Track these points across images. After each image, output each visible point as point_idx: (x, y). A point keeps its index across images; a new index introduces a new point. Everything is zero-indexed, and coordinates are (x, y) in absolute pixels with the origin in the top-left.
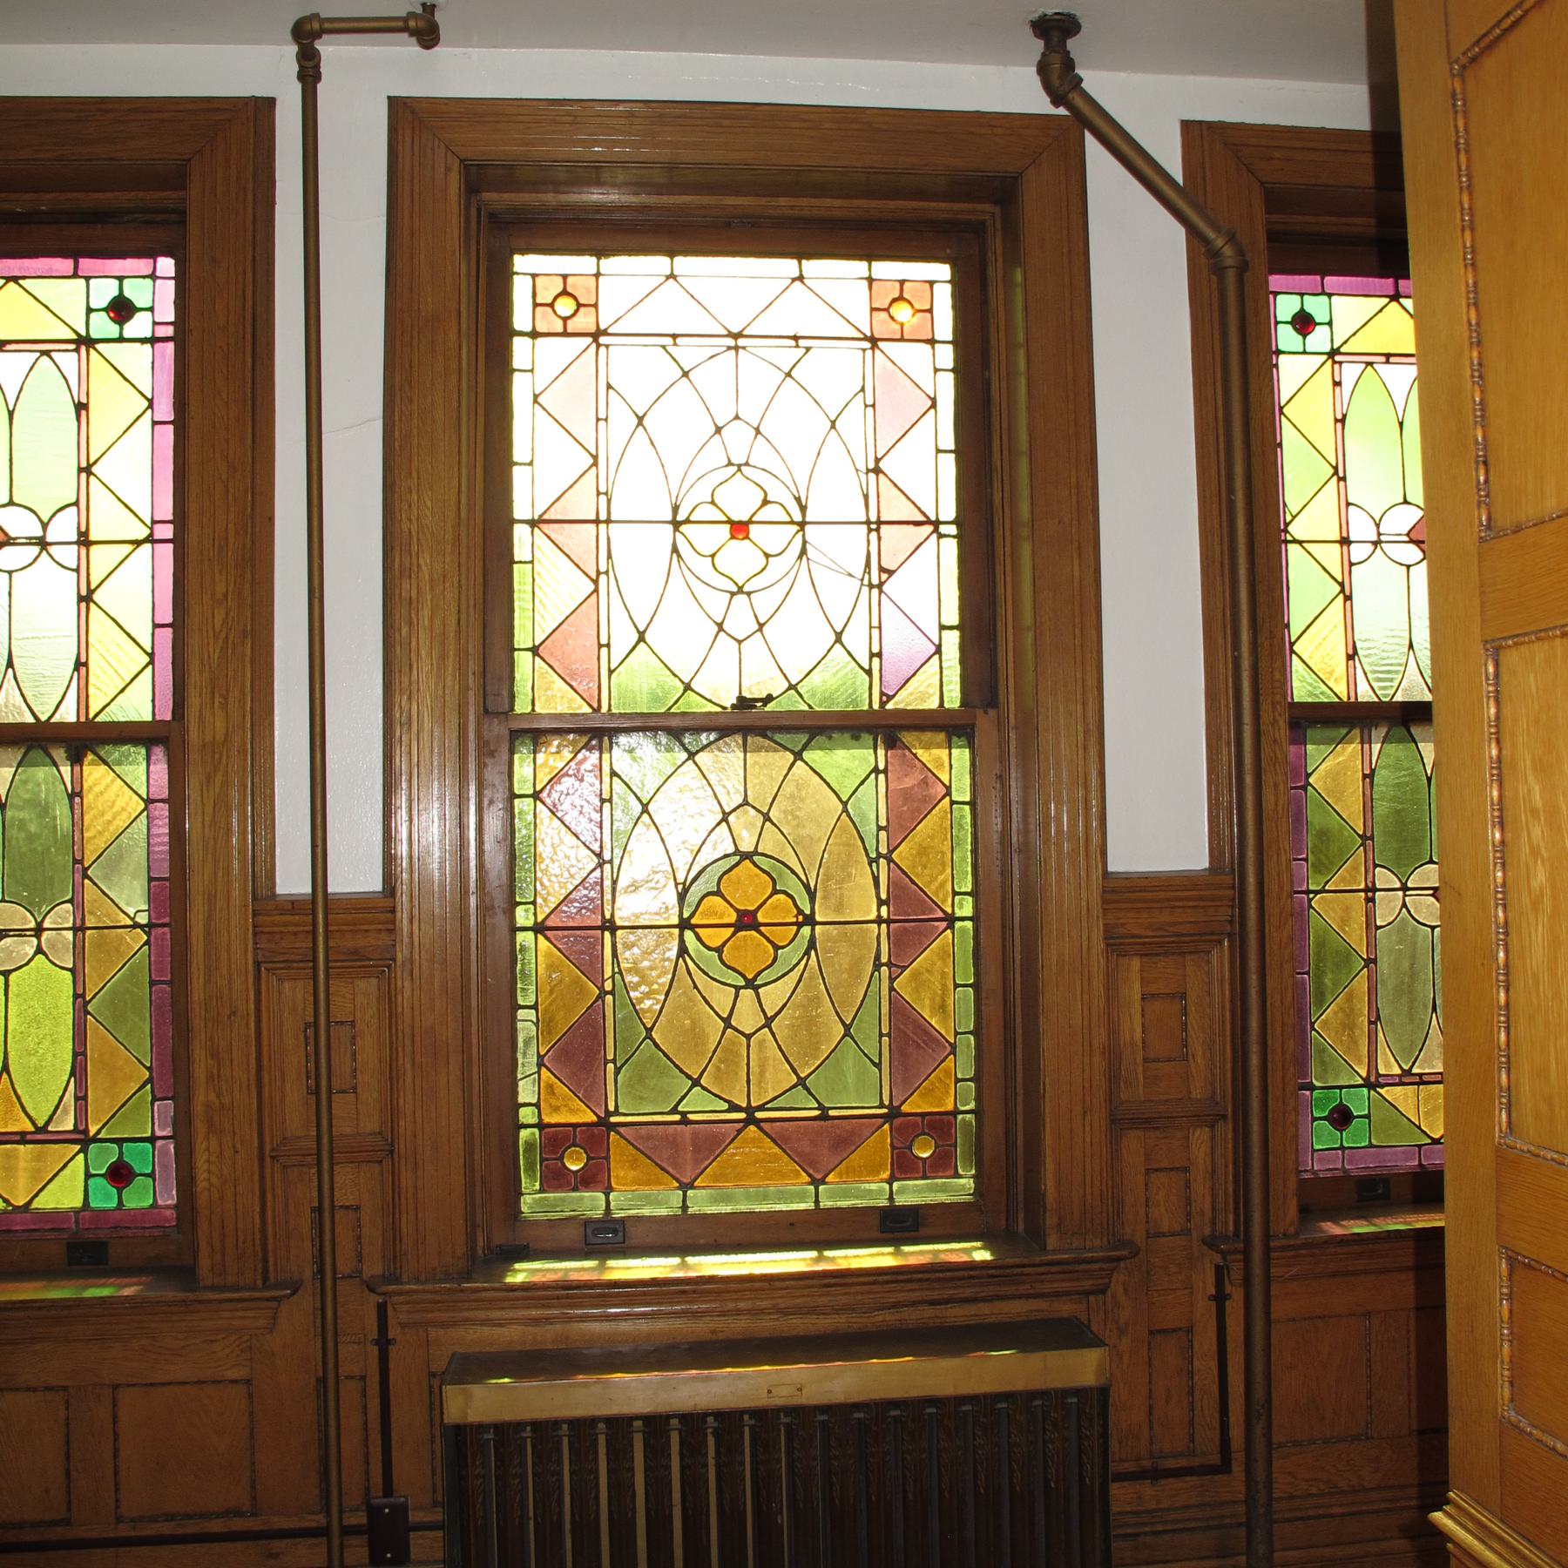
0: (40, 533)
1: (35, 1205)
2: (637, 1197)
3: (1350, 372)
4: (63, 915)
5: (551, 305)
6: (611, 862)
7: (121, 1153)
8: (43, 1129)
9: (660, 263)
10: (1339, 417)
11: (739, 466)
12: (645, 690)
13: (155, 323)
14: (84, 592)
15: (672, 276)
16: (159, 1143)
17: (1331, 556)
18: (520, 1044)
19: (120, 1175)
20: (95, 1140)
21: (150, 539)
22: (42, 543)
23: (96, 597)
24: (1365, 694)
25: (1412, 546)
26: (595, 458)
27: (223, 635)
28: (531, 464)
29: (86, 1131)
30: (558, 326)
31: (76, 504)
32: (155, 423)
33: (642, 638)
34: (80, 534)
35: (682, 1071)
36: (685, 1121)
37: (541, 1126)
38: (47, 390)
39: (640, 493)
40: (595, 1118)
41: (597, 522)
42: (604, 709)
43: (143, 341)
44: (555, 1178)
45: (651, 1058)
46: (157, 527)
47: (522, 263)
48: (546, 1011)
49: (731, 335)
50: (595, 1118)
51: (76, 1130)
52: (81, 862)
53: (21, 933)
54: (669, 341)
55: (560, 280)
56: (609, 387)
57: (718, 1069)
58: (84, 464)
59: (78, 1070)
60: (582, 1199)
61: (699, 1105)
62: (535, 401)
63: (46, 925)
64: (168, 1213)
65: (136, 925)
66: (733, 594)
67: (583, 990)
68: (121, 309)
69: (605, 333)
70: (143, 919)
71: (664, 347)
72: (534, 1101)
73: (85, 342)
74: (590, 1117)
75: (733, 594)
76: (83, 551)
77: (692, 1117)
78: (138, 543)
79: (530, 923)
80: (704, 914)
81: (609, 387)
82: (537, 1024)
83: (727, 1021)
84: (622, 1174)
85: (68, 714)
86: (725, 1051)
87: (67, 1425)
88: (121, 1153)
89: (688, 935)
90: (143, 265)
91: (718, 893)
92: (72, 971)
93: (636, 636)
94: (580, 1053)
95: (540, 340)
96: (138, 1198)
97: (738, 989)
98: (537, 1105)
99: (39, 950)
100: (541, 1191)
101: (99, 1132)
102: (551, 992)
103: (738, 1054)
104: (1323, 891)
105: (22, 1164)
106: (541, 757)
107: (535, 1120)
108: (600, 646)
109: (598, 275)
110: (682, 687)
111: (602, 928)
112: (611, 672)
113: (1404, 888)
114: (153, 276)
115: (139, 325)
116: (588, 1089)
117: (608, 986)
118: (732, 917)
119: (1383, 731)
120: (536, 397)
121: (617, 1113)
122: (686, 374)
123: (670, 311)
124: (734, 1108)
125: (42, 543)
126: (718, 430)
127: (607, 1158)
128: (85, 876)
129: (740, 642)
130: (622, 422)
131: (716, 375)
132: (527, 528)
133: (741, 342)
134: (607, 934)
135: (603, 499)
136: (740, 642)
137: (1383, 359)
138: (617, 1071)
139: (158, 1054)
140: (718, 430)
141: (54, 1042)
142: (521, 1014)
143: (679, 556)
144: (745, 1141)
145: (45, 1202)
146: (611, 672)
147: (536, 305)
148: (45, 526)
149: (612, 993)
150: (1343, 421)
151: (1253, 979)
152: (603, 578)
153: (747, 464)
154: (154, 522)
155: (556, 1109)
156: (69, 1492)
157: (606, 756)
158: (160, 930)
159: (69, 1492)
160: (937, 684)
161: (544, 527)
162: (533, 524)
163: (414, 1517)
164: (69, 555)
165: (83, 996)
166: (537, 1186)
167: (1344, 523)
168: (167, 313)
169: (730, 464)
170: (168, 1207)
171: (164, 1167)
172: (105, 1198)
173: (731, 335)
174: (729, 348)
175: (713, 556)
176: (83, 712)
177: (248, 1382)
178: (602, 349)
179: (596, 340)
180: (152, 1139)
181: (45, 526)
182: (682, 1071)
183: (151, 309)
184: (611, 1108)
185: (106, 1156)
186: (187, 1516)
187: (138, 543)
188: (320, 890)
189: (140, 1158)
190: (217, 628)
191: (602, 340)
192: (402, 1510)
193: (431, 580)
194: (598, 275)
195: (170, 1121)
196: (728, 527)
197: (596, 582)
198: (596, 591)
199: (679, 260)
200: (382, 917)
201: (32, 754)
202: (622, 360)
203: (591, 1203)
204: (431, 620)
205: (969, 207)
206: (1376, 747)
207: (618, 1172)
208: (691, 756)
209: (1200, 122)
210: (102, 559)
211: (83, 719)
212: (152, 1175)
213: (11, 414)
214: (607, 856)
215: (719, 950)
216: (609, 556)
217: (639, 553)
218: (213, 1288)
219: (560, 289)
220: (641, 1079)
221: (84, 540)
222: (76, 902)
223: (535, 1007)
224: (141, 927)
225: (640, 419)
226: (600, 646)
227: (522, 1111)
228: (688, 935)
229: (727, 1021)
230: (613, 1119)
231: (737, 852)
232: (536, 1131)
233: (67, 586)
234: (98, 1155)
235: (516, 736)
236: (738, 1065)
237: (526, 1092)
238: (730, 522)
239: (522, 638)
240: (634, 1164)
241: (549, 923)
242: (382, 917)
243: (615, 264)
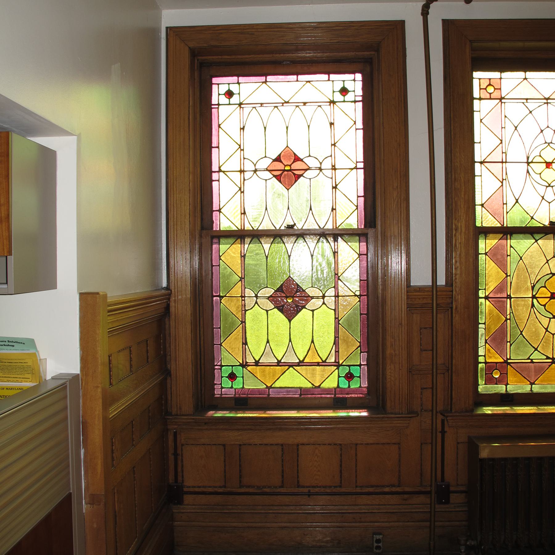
0: (319, 166)
1: (321, 386)
2: (516, 386)
3: (247, 109)
4: (331, 292)
5: (485, 89)
6: (510, 276)
7: (350, 370)
8: (325, 362)
9: (521, 74)
10: (242, 127)
11: (549, 143)
12: (518, 219)
13: (355, 96)
14: (334, 186)
15: (525, 79)
16: (362, 367)
17: (236, 177)
18: (480, 336)
19: (349, 377)
20: (341, 365)
21: (356, 168)
22: (320, 169)
23: (338, 187)
24: (248, 227)
25: (268, 172)
26: (501, 141)
27: (396, 200)
28: (480, 143)
29: (338, 362)
30: (488, 96)
31: (331, 156)
32: (356, 129)
33: (517, 202)
34: (333, 166)
35: (531, 345)
36: (532, 362)
37: (486, 363)
38: (320, 118)
39: (516, 153)
40: (503, 361)
41: (502, 162)
42: (505, 225)
43: (352, 102)
44: (490, 380)
45: (522, 341)
46: (358, 164)
47: (476, 74)
48: (488, 325)
49: (545, 99)
50: (503, 361)
51: (335, 362)
52: (337, 274)
53: (318, 298)
54: (525, 101)
55: (488, 80)
56: (505, 117)
57: (543, 345)
58: (333, 143)
59: (336, 343)
60: (498, 387)
61: (537, 356)
62: (481, 122)
63: (326, 295)
64: (365, 389)
65: (356, 295)
66: (547, 187)
67: (499, 318)
68: (344, 91)
69: (504, 98)
70: (358, 293)
71: (523, 103)
72: (484, 354)
73: (333, 102)
74: (502, 360)
75: (547, 187)
76: (334, 171)
77: (534, 361)
78: (352, 169)
79: (484, 296)
80: (540, 294)
81: (505, 117)
82: (485, 329)
83: (546, 329)
84: (511, 379)
85: (330, 226)
86: (546, 339)
87: (341, 456)
88: (350, 370)
89: (535, 300)
90: (351, 76)
91: (545, 287)
92: (335, 310)
93: (515, 201)
94: (499, 339)
95: (482, 101)
96: (355, 384)
97: (550, 318)
98: (485, 356)
99: (324, 303)
100: (485, 384)
101: (343, 362)
102: (490, 319)
103: (549, 340)
104: (225, 296)
105: (318, 373)
106: (487, 241)
107: (484, 361)
108: (504, 204)
109: (501, 78)
110: (530, 218)
111: (507, 298)
112: (507, 213)
113: (256, 296)
114: (354, 80)
115: (350, 97)
116: (501, 351)
117: (508, 317)
118: (549, 295)
119: (249, 240)
120: (481, 120)
121: (510, 359)
122: (531, 112)
123: (524, 91)
124: (548, 358)
125: (320, 169)
126: (542, 131)
127: (507, 374)
128: (339, 279)
129: (550, 203)
130: (510, 128)
131: (541, 112)
132: (479, 164)
133: (549, 101)
134: (508, 300)
135: (504, 154)
136: (550, 203)
137: (260, 105)
138: (511, 345)
139: (363, 338)
140: (542, 131)
141: (328, 333)
142: (480, 326)
143: (529, 174)
144: (551, 369)
145: (325, 385)
146: (507, 213)
147: (480, 89)
148: (321, 163)
149: (510, 319)
150: (243, 129)
151: (435, 323)
152: (504, 181)
153: (551, 143)
154: (357, 162)
155: (490, 357)
156: (341, 477)
157: (509, 241)
158: (363, 297)
159: (341, 477)
160: (352, 219)
161: (486, 164)
162: (481, 163)
163: (452, 489)
164: (329, 173)
165: (338, 318)
166: (484, 383)
167: (242, 163)
168: (359, 92)
169: (546, 143)
170: (365, 387)
171: (364, 374)
172: (344, 384)
173: (545, 99)
174: (545, 103)
175: (540, 174)
176: (335, 225)
177: (399, 444)
178: (503, 104)
179: (501, 101)
180: (360, 365)
181: (321, 163)
182: (531, 345)
183: (354, 91)
184: (508, 357)
185: (344, 371)
186: (377, 486)
187: (352, 169)
188: (435, 284)
189: (356, 371)
190: (395, 198)
191: (503, 101)
192: (448, 486)
193: (464, 182)
194: (501, 78)
195: (366, 359)
196: (545, 164)
197: (502, 182)
198: (502, 185)
199: (528, 73)
200: (448, 293)
201: (254, 240)
202: (510, 108)
203: (501, 389)
204: (464, 195)
205: (366, 52)
206: (246, 246)
207: (510, 378)
208: (536, 241)
209: (448, 20)
210: (340, 174)
211: (335, 227)
212: (360, 377)
213: (309, 126)
214: (508, 274)
215: (544, 306)
216: (506, 174)
217: (516, 173)
218: (392, 413)
219: (488, 83)
220: (518, 348)
221: (334, 168)
222: (336, 287)
223: (485, 324)
224: (357, 296)
225: (516, 128)
226: (504, 204)
227: (480, 358)
228: (535, 300)
229: (546, 329)
230: (509, 361)
231: (551, 273)
232: (484, 364)
233: (329, 184)
234: (342, 370)
235: (213, 237)
236: (549, 344)
237: (481, 352)
238: (546, 162)
239: (478, 201)
240: (515, 376)
241: (490, 296)
242: (448, 293)
243: (506, 75)
